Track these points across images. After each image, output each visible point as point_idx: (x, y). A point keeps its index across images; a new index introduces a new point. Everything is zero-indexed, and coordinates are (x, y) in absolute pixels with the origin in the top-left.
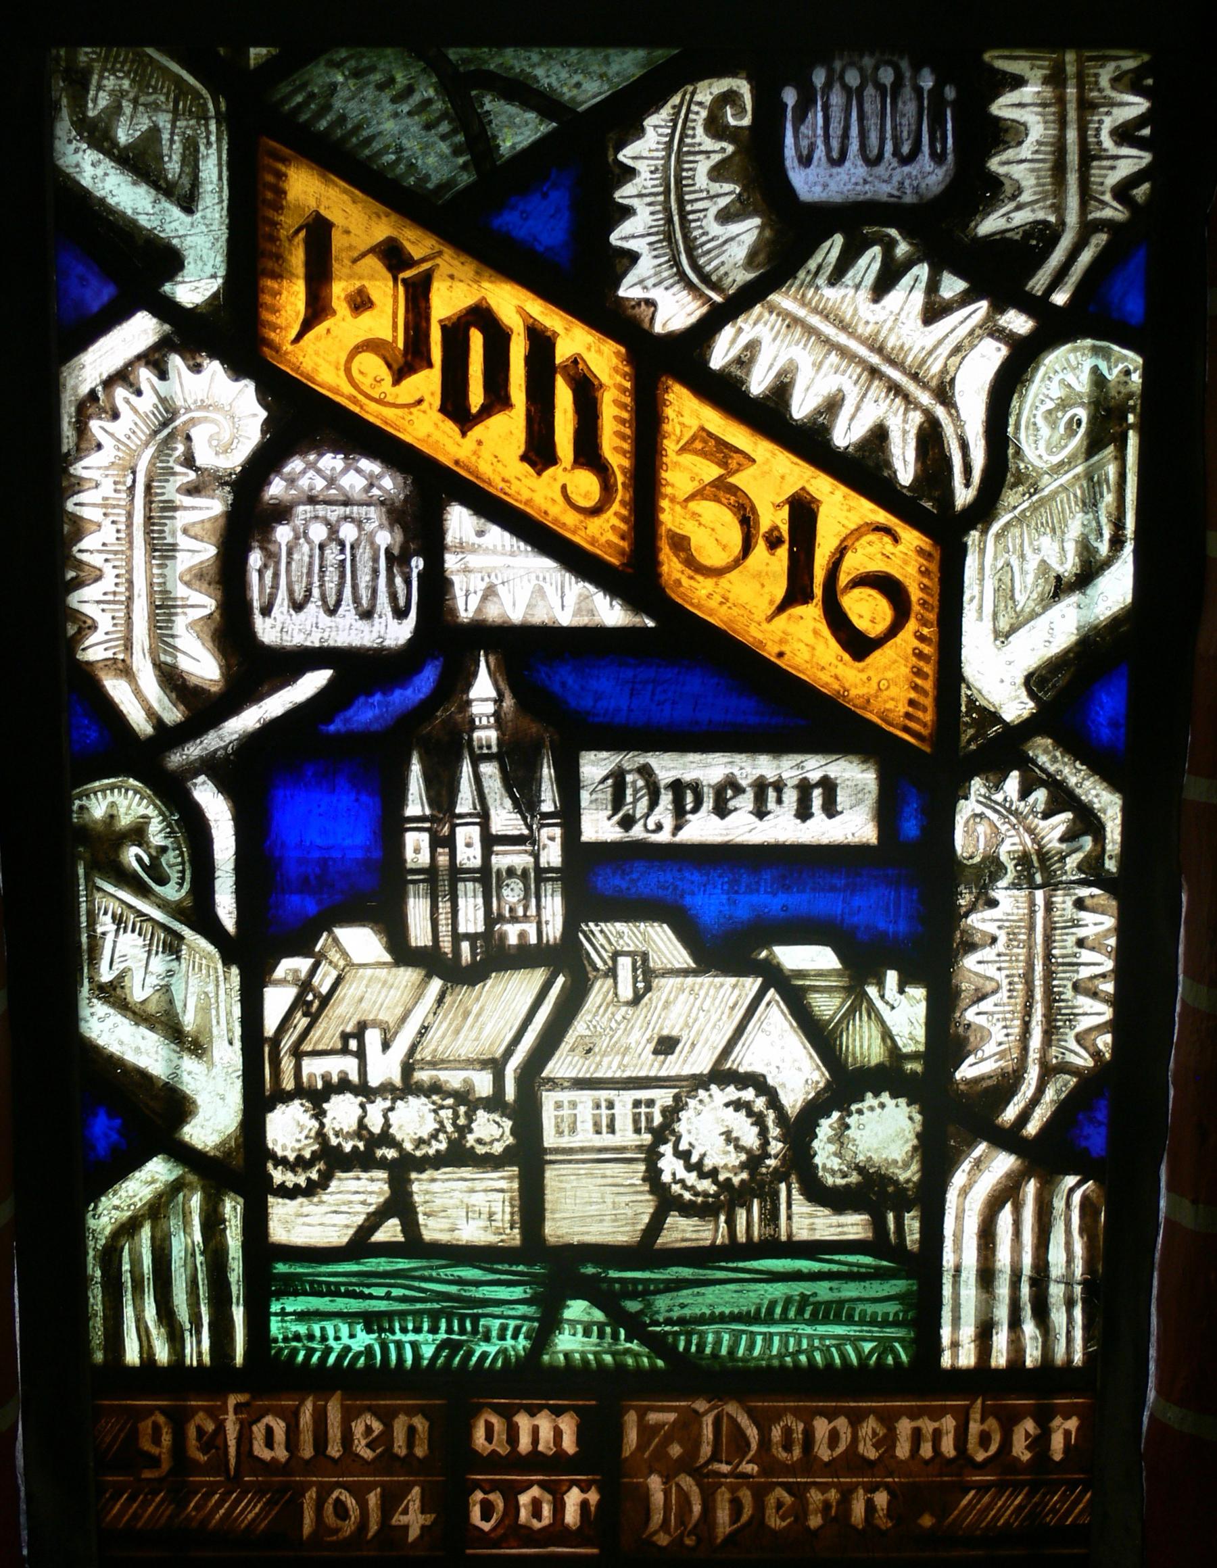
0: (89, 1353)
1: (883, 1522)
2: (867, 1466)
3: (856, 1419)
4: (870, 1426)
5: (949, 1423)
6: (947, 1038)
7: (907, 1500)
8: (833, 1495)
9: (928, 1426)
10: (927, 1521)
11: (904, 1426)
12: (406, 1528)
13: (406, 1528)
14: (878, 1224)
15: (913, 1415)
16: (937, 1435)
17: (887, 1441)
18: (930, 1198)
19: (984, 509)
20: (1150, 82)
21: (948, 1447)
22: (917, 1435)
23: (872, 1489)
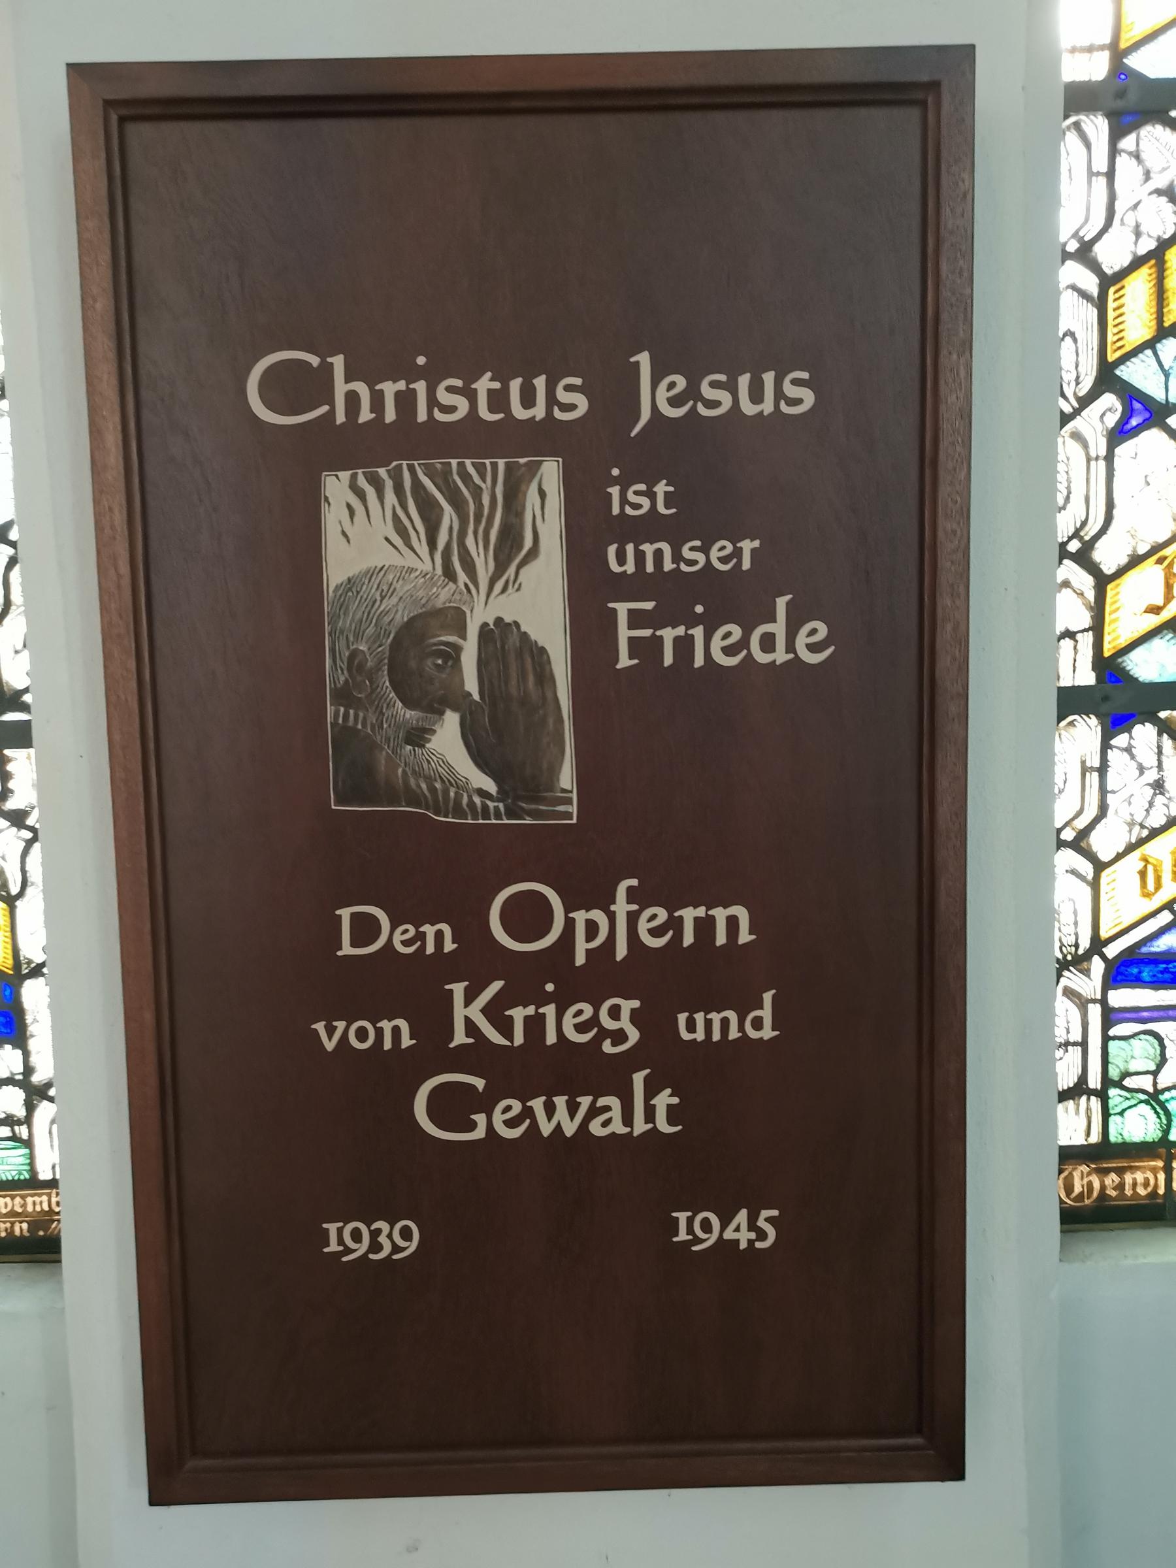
0: (1046, 793)
1: (26, 1234)
2: (18, 1214)
3: (13, 1198)
4: (18, 1200)
5: (45, 1198)
6: (28, 1070)
7: (34, 1225)
8: (8, 1225)
9: (37, 1199)
10: (41, 1233)
11: (29, 1200)
12: (737, 1241)
13: (737, 1241)
14: (13, 1131)
15: (32, 1195)
16: (41, 1203)
17: (24, 1206)
18: (28, 1120)
19: (21, 894)
20: (421, 360)
21: (46, 1208)
22: (34, 1203)
23: (21, 1222)
